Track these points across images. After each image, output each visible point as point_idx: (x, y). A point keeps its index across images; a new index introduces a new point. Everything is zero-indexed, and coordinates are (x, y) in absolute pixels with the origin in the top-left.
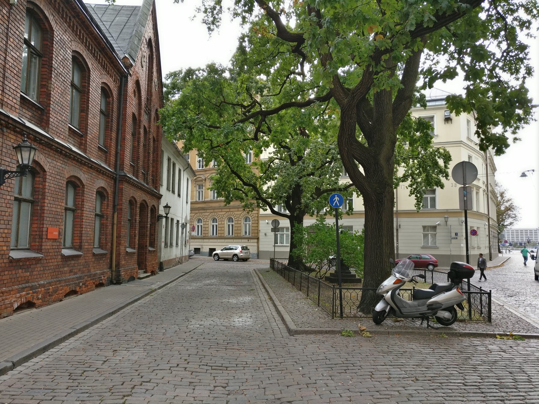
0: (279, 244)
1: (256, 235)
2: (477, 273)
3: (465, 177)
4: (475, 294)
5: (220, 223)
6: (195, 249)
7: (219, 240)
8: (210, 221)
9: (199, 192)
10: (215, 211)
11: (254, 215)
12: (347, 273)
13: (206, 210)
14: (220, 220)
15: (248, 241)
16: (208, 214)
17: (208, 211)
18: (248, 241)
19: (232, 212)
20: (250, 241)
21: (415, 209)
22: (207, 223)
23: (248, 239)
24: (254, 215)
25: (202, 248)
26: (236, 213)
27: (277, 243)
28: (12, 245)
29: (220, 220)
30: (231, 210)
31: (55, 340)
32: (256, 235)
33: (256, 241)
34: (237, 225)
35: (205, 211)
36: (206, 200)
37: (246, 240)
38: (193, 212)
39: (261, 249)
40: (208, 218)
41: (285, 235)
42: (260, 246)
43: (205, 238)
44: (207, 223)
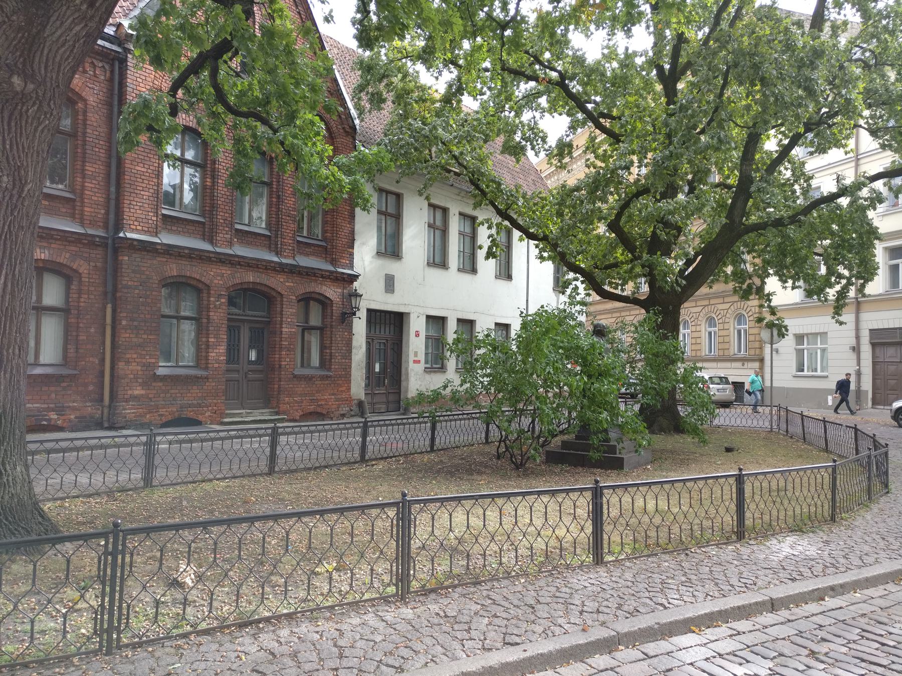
0: (806, 373)
1: (758, 352)
4: (692, 483)
5: (721, 326)
7: (720, 365)
11: (753, 309)
14: (720, 321)
15: (743, 365)
16: (727, 306)
18: (743, 365)
20: (746, 366)
21: (481, 337)
23: (743, 360)
24: (753, 309)
26: (721, 307)
27: (803, 370)
28: (31, 359)
29: (720, 321)
30: (712, 302)
31: (690, 615)
32: (758, 352)
33: (757, 365)
34: (722, 333)
37: (739, 364)
39: (774, 385)
40: (700, 318)
41: (806, 351)
42: (774, 382)
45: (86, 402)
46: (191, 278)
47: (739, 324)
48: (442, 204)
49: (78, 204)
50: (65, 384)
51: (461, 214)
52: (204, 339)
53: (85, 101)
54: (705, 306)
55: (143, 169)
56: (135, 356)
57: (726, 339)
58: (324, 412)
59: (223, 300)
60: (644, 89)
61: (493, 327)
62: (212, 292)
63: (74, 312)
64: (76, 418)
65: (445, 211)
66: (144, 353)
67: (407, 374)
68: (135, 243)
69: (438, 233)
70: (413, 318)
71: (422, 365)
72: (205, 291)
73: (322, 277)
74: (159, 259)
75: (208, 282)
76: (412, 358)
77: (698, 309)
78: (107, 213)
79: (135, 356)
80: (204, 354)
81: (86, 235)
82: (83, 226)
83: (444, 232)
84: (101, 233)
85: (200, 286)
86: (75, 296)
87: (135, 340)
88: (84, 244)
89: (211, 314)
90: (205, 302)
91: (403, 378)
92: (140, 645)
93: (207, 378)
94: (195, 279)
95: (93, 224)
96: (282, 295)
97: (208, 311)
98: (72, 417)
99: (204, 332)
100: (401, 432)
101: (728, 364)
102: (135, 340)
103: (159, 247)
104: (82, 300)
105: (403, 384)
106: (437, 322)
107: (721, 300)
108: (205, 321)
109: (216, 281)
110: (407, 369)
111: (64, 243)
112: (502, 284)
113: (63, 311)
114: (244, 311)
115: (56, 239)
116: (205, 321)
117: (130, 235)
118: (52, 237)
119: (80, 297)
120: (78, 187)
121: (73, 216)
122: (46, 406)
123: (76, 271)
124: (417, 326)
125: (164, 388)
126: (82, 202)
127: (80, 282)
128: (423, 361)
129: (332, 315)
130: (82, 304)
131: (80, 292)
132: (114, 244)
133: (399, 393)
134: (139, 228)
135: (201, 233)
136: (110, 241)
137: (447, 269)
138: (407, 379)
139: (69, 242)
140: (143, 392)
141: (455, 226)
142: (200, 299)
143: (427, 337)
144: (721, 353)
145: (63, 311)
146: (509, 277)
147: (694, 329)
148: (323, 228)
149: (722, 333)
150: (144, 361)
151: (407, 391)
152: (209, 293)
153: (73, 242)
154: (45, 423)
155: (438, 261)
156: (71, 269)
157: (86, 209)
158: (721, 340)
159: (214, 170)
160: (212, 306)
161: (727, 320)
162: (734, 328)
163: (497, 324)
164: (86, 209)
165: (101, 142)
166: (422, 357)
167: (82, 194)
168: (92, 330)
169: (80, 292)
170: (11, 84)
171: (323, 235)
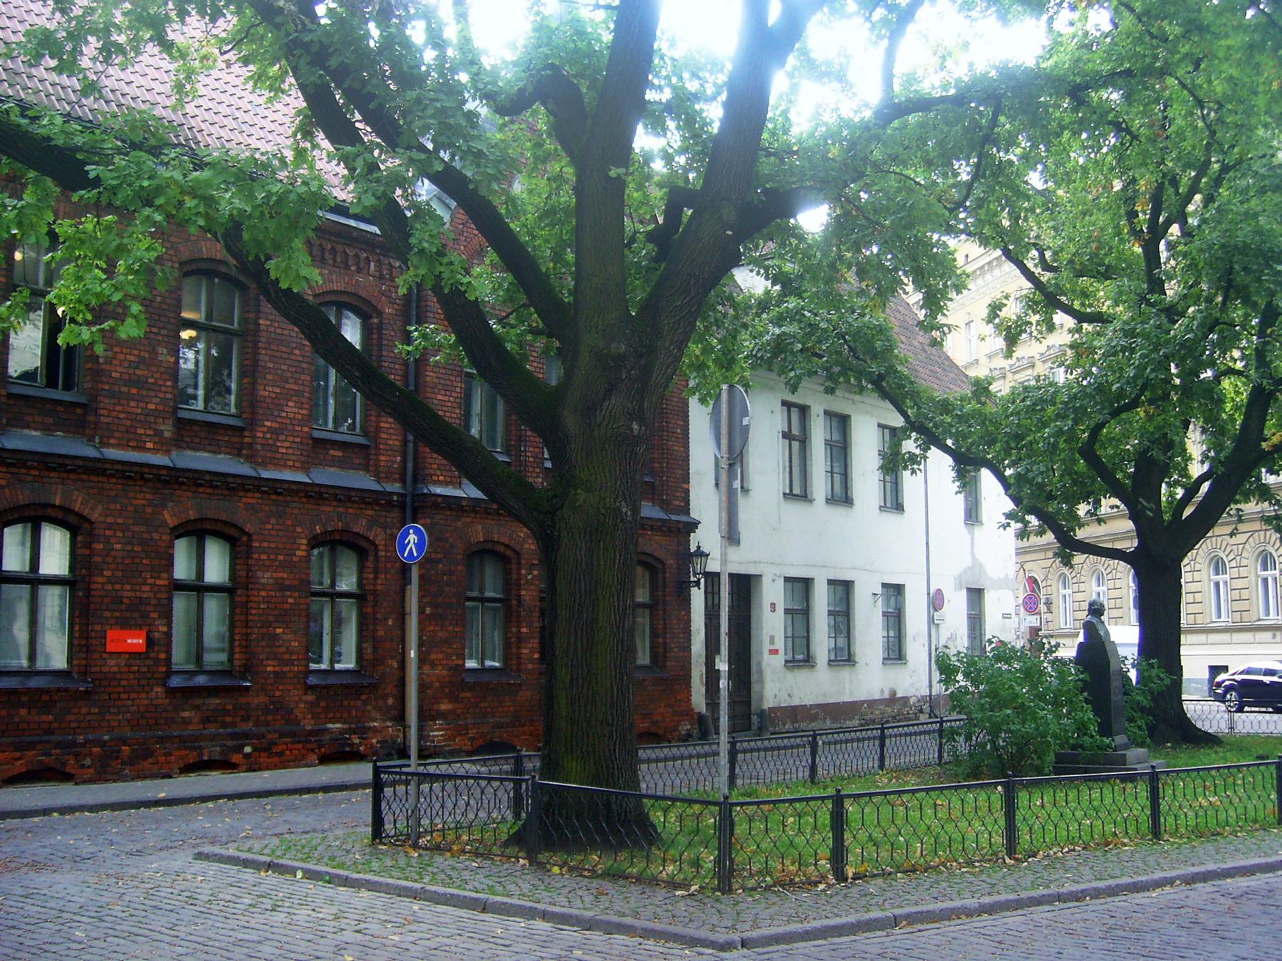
15: (1274, 636)
18: (1274, 636)
19: (1220, 539)
45: (386, 721)
46: (498, 542)
47: (1265, 569)
48: (800, 402)
49: (373, 452)
50: (364, 697)
51: (826, 412)
52: (514, 630)
53: (380, 313)
55: (444, 398)
56: (440, 656)
57: (1245, 594)
58: (660, 732)
59: (536, 573)
60: (1151, 291)
61: (879, 590)
63: (370, 598)
64: (378, 742)
65: (804, 410)
66: (449, 651)
67: (760, 672)
68: (440, 500)
69: (796, 445)
70: (766, 581)
71: (779, 660)
72: (514, 561)
73: (652, 528)
74: (463, 519)
75: (518, 548)
76: (766, 647)
78: (404, 461)
79: (440, 656)
80: (514, 651)
81: (384, 493)
82: (379, 483)
83: (804, 440)
84: (395, 487)
85: (508, 553)
86: (371, 576)
87: (440, 634)
88: (381, 505)
89: (523, 593)
90: (514, 577)
91: (754, 677)
93: (520, 685)
94: (503, 544)
95: (388, 478)
97: (519, 590)
98: (374, 741)
99: (514, 619)
100: (782, 757)
101: (1248, 636)
102: (440, 634)
103: (465, 503)
104: (379, 581)
105: (755, 688)
106: (801, 587)
108: (514, 602)
109: (527, 546)
110: (759, 664)
111: (362, 506)
112: (891, 518)
113: (359, 597)
115: (354, 502)
116: (514, 602)
117: (438, 490)
118: (349, 499)
119: (376, 578)
120: (372, 429)
121: (366, 468)
122: (347, 726)
123: (372, 543)
124: (772, 595)
126: (377, 448)
127: (377, 558)
128: (782, 651)
129: (664, 585)
130: (379, 588)
131: (376, 571)
132: (413, 502)
133: (749, 703)
134: (441, 478)
136: (409, 499)
137: (811, 501)
138: (761, 681)
139: (366, 503)
140: (450, 706)
141: (819, 433)
142: (507, 573)
143: (787, 611)
145: (359, 597)
146: (899, 507)
150: (450, 662)
151: (761, 699)
152: (519, 564)
153: (369, 504)
154: (348, 749)
155: (799, 493)
156: (367, 539)
157: (383, 458)
158: (1236, 594)
161: (1244, 562)
162: (1257, 576)
163: (884, 585)
164: (383, 458)
165: (397, 366)
166: (780, 644)
167: (377, 437)
168: (390, 622)
169: (376, 571)
170: (631, 430)
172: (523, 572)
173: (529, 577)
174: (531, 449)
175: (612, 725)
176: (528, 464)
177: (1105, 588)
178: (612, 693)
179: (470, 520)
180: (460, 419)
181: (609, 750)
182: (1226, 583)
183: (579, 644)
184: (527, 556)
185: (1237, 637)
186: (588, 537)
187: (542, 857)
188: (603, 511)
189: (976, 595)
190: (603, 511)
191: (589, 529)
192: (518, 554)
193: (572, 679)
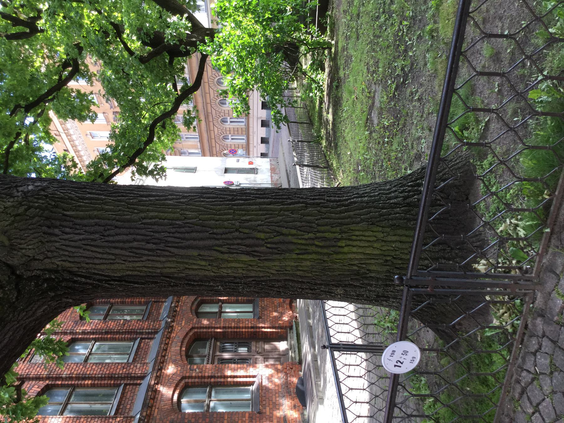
2: (82, 360)
3: (90, 398)
6: (262, 126)
8: (226, 143)
9: (187, 138)
10: (208, 101)
11: (213, 73)
12: (221, 377)
13: (207, 113)
17: (210, 111)
19: (210, 80)
22: (227, 112)
24: (213, 73)
25: (261, 117)
34: (232, 132)
35: (210, 114)
36: (199, 147)
38: (215, 153)
40: (220, 111)
43: (247, 131)
44: (227, 112)
54: (209, 86)
62: (188, 375)
74: (156, 414)
77: (216, 129)
92: (511, 172)
96: (193, 328)
103: (144, 414)
107: (208, 95)
114: (205, 356)
125: (271, 406)
135: (134, 387)
144: (244, 133)
147: (228, 132)
148: (136, 305)
149: (232, 132)
152: (189, 377)
158: (236, 133)
159: (78, 378)
160: (200, 375)
171: (143, 305)
172: (194, 375)
173: (197, 370)
174: (118, 371)
175: (307, 204)
176: (127, 372)
177: (230, 135)
178: (264, 203)
179: (156, 410)
180: (88, 418)
181: (338, 206)
182: (232, 136)
183: (201, 243)
184: (185, 372)
185: (251, 133)
186: (57, 231)
187: (415, 324)
188: (21, 210)
189: (226, 171)
190: (21, 210)
191: (44, 228)
192: (183, 378)
193: (248, 254)
